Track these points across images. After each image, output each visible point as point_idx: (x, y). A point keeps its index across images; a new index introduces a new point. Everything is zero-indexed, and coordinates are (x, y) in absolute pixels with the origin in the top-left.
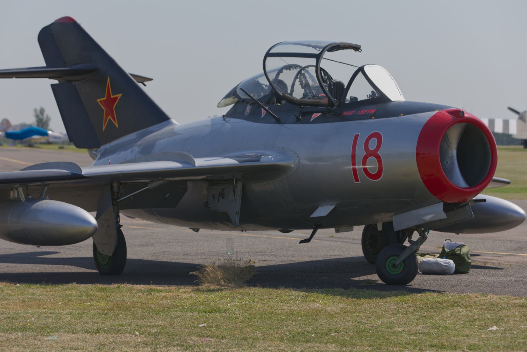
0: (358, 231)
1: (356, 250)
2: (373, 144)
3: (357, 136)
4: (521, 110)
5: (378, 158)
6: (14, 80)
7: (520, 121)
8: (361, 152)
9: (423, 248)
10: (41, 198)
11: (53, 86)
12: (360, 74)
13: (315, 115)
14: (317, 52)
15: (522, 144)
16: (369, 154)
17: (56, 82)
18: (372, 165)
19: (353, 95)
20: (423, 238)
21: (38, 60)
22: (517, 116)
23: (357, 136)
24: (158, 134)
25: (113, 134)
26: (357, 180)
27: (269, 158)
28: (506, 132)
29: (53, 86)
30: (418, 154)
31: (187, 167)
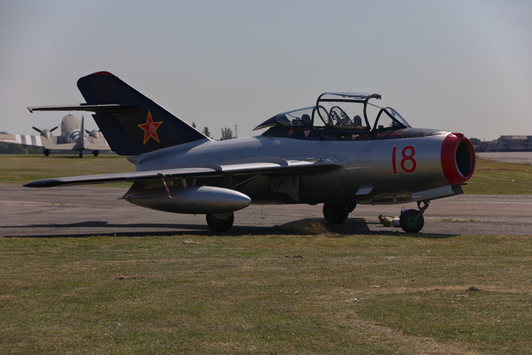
0: (321, 205)
1: (321, 215)
2: (408, 153)
3: (395, 149)
4: (41, 129)
5: (413, 160)
6: (39, 111)
7: (43, 137)
8: (399, 158)
9: (426, 211)
10: (202, 185)
11: (93, 115)
12: (383, 112)
13: (354, 136)
14: (364, 99)
15: (93, 153)
16: (406, 158)
17: (94, 113)
18: (409, 164)
19: (381, 125)
20: (426, 206)
21: (80, 99)
22: (39, 133)
23: (395, 149)
24: (200, 148)
25: (152, 146)
26: (395, 172)
27: (328, 161)
28: (24, 143)
29: (93, 115)
30: (441, 159)
31: (283, 166)
